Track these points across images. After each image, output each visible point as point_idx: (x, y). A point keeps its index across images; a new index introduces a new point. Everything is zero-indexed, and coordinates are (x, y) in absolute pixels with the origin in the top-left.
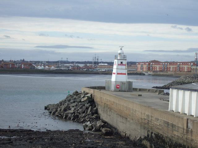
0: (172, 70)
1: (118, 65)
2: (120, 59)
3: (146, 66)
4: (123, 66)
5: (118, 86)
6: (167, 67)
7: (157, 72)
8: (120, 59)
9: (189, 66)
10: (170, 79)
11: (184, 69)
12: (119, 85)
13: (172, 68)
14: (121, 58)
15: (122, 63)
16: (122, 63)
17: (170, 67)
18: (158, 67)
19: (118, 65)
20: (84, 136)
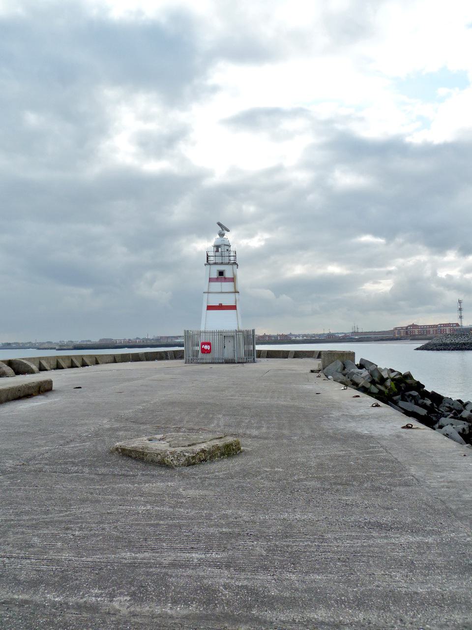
0: (432, 333)
1: (211, 280)
2: (215, 264)
3: (403, 331)
4: (224, 284)
5: (206, 347)
6: (423, 331)
7: (415, 335)
8: (215, 264)
9: (452, 328)
10: (420, 343)
11: (446, 331)
12: (209, 344)
13: (432, 331)
14: (219, 260)
15: (221, 273)
16: (221, 273)
17: (429, 330)
18: (416, 331)
19: (211, 280)
20: (394, 578)
